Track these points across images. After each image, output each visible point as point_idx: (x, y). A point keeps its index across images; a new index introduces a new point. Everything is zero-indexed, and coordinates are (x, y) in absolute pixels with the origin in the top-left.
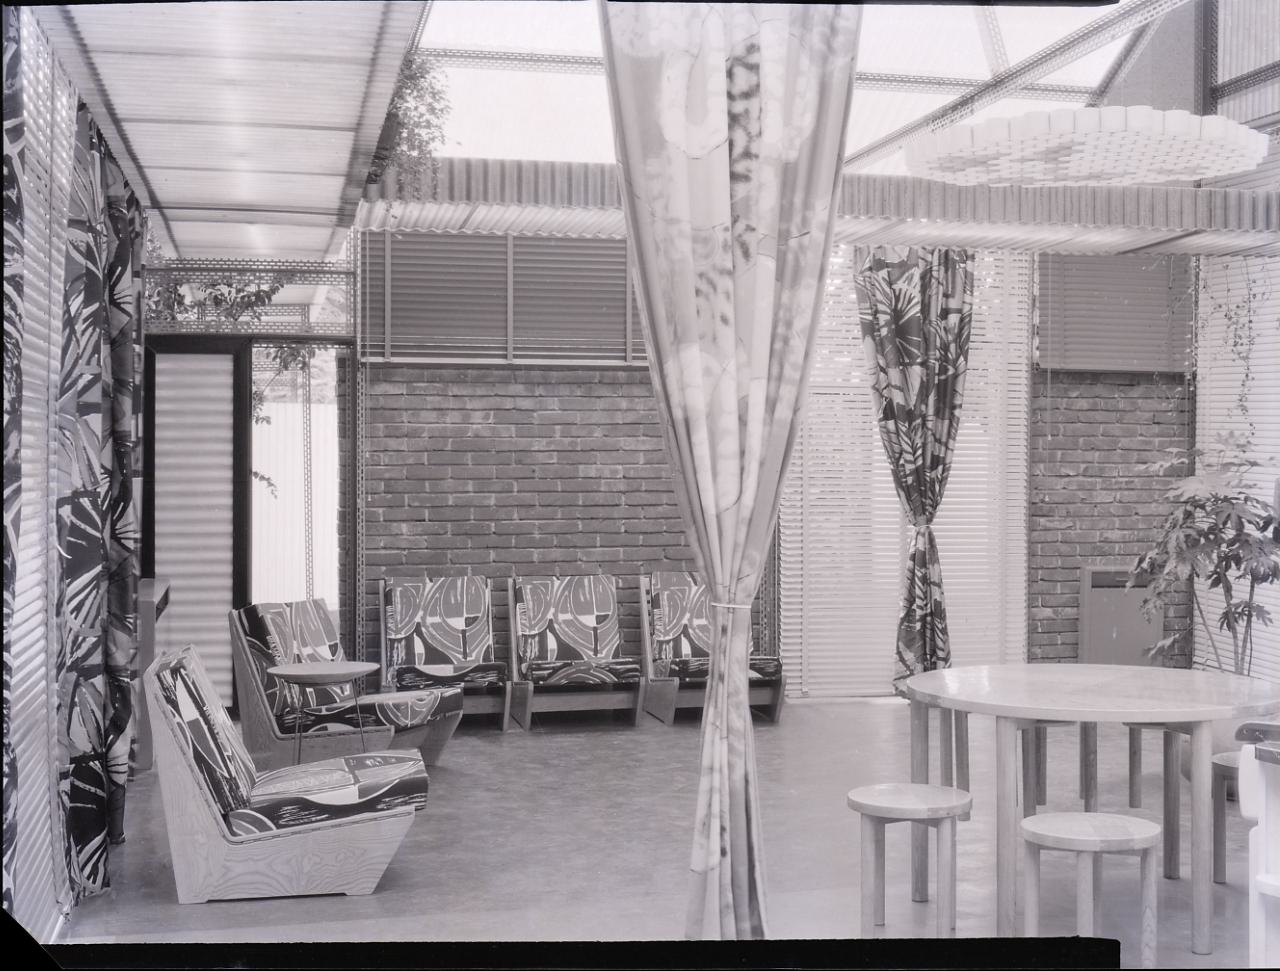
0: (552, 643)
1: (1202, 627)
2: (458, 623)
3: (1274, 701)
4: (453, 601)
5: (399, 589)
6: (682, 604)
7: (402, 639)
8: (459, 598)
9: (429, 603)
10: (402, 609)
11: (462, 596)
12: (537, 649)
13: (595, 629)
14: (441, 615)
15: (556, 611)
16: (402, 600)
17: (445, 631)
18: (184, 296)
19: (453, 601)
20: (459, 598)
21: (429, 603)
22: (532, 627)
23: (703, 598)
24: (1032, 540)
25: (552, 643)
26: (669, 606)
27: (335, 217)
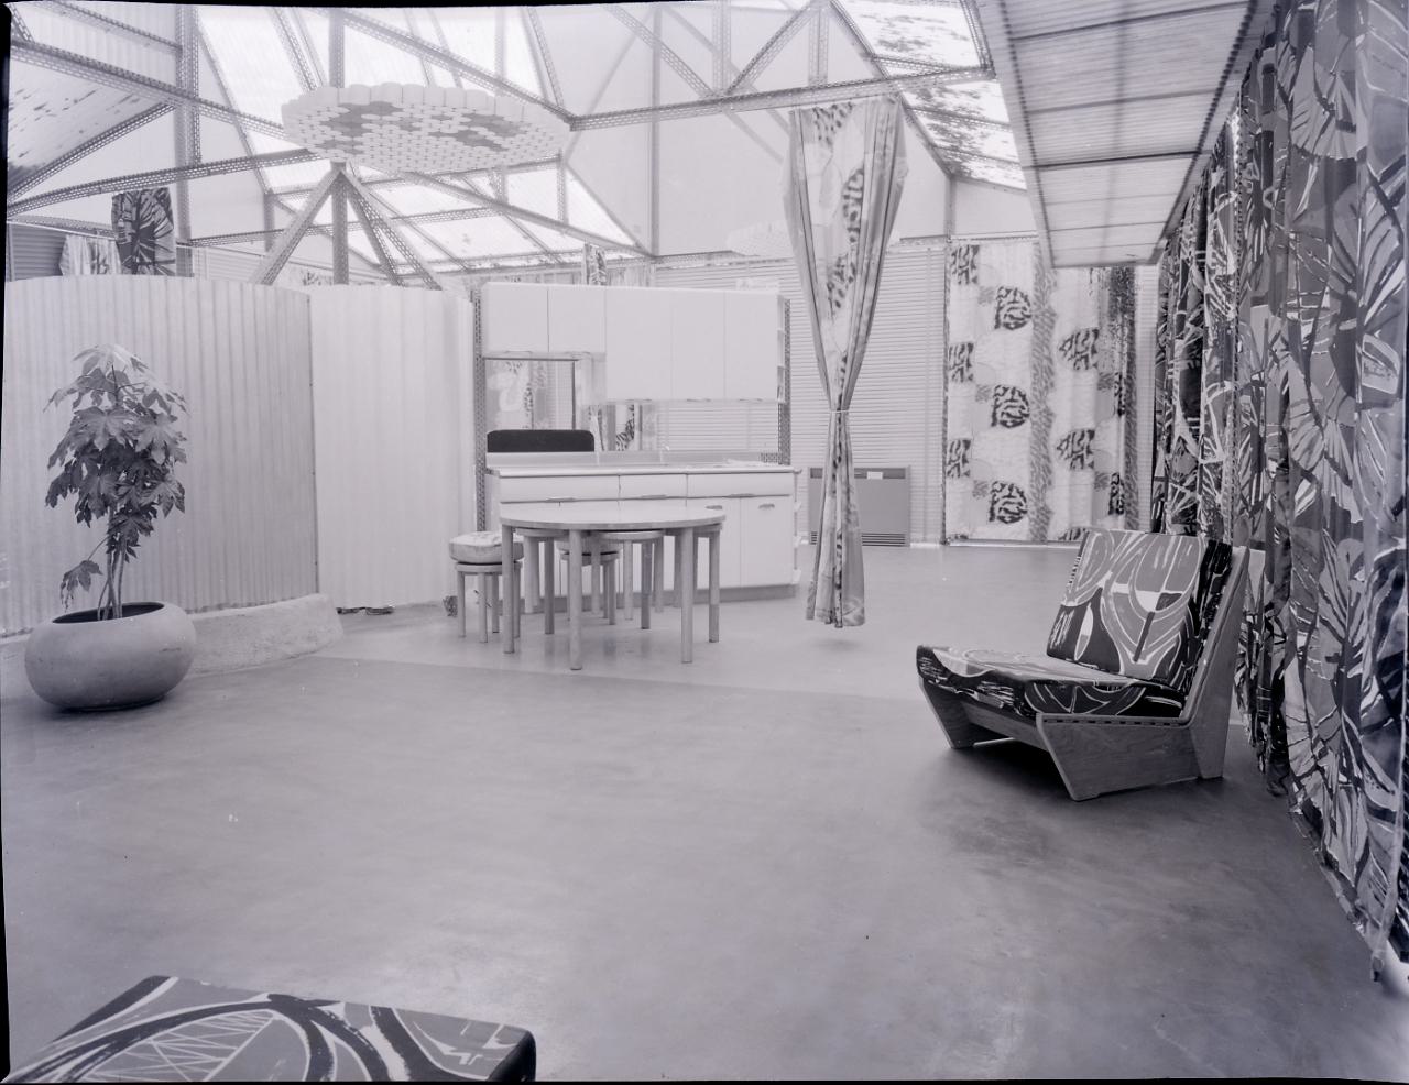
0: (1087, 628)
1: (1067, 246)
2: (1149, 600)
3: (1285, 29)
4: (1155, 565)
5: (1098, 534)
6: (1109, 556)
7: (1072, 608)
8: (1166, 560)
9: (1125, 561)
10: (1089, 564)
11: (1170, 558)
12: (1065, 632)
13: (1151, 616)
14: (1132, 583)
15: (1113, 577)
16: (1093, 552)
18: (185, 272)
19: (1155, 565)
20: (1166, 560)
21: (1125, 561)
22: (1071, 598)
23: (1139, 552)
24: (1042, 158)
25: (1087, 628)
26: (1092, 557)
27: (277, 228)
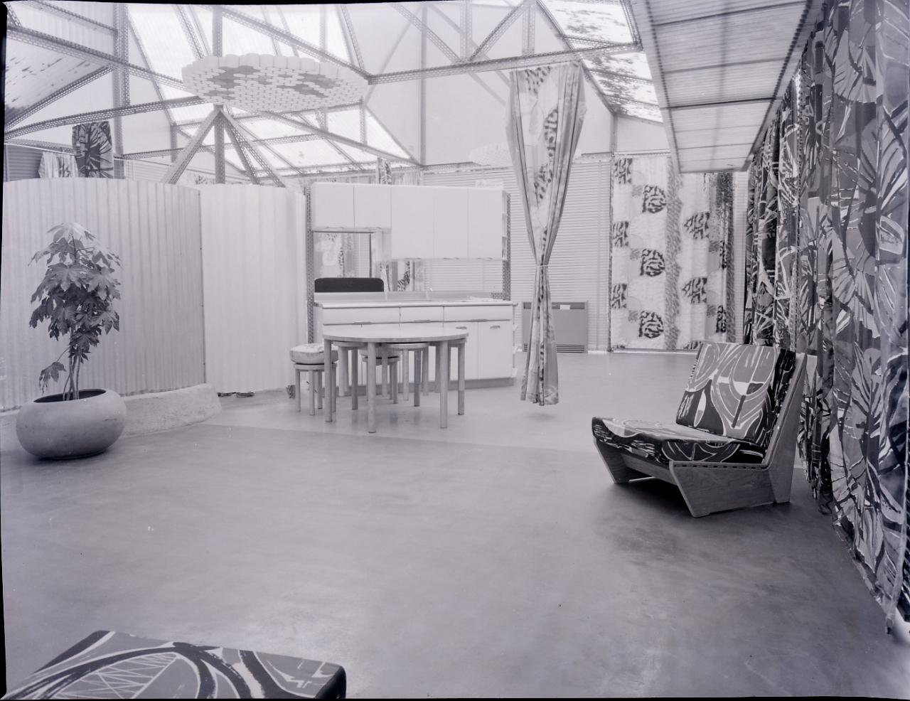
0: (702, 406)
4: (746, 365)
5: (709, 345)
6: (716, 359)
7: (692, 393)
8: (753, 362)
9: (727, 362)
10: (703, 364)
11: (756, 360)
12: (688, 409)
13: (743, 398)
14: (731, 377)
15: (719, 373)
17: (728, 392)
18: (120, 175)
19: (746, 365)
20: (753, 362)
21: (727, 362)
22: (692, 386)
23: (736, 356)
24: (673, 102)
25: (702, 406)
26: (705, 360)
